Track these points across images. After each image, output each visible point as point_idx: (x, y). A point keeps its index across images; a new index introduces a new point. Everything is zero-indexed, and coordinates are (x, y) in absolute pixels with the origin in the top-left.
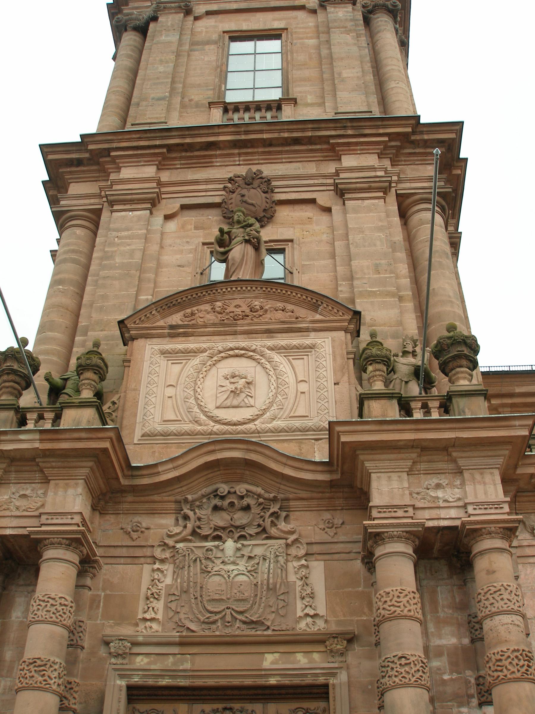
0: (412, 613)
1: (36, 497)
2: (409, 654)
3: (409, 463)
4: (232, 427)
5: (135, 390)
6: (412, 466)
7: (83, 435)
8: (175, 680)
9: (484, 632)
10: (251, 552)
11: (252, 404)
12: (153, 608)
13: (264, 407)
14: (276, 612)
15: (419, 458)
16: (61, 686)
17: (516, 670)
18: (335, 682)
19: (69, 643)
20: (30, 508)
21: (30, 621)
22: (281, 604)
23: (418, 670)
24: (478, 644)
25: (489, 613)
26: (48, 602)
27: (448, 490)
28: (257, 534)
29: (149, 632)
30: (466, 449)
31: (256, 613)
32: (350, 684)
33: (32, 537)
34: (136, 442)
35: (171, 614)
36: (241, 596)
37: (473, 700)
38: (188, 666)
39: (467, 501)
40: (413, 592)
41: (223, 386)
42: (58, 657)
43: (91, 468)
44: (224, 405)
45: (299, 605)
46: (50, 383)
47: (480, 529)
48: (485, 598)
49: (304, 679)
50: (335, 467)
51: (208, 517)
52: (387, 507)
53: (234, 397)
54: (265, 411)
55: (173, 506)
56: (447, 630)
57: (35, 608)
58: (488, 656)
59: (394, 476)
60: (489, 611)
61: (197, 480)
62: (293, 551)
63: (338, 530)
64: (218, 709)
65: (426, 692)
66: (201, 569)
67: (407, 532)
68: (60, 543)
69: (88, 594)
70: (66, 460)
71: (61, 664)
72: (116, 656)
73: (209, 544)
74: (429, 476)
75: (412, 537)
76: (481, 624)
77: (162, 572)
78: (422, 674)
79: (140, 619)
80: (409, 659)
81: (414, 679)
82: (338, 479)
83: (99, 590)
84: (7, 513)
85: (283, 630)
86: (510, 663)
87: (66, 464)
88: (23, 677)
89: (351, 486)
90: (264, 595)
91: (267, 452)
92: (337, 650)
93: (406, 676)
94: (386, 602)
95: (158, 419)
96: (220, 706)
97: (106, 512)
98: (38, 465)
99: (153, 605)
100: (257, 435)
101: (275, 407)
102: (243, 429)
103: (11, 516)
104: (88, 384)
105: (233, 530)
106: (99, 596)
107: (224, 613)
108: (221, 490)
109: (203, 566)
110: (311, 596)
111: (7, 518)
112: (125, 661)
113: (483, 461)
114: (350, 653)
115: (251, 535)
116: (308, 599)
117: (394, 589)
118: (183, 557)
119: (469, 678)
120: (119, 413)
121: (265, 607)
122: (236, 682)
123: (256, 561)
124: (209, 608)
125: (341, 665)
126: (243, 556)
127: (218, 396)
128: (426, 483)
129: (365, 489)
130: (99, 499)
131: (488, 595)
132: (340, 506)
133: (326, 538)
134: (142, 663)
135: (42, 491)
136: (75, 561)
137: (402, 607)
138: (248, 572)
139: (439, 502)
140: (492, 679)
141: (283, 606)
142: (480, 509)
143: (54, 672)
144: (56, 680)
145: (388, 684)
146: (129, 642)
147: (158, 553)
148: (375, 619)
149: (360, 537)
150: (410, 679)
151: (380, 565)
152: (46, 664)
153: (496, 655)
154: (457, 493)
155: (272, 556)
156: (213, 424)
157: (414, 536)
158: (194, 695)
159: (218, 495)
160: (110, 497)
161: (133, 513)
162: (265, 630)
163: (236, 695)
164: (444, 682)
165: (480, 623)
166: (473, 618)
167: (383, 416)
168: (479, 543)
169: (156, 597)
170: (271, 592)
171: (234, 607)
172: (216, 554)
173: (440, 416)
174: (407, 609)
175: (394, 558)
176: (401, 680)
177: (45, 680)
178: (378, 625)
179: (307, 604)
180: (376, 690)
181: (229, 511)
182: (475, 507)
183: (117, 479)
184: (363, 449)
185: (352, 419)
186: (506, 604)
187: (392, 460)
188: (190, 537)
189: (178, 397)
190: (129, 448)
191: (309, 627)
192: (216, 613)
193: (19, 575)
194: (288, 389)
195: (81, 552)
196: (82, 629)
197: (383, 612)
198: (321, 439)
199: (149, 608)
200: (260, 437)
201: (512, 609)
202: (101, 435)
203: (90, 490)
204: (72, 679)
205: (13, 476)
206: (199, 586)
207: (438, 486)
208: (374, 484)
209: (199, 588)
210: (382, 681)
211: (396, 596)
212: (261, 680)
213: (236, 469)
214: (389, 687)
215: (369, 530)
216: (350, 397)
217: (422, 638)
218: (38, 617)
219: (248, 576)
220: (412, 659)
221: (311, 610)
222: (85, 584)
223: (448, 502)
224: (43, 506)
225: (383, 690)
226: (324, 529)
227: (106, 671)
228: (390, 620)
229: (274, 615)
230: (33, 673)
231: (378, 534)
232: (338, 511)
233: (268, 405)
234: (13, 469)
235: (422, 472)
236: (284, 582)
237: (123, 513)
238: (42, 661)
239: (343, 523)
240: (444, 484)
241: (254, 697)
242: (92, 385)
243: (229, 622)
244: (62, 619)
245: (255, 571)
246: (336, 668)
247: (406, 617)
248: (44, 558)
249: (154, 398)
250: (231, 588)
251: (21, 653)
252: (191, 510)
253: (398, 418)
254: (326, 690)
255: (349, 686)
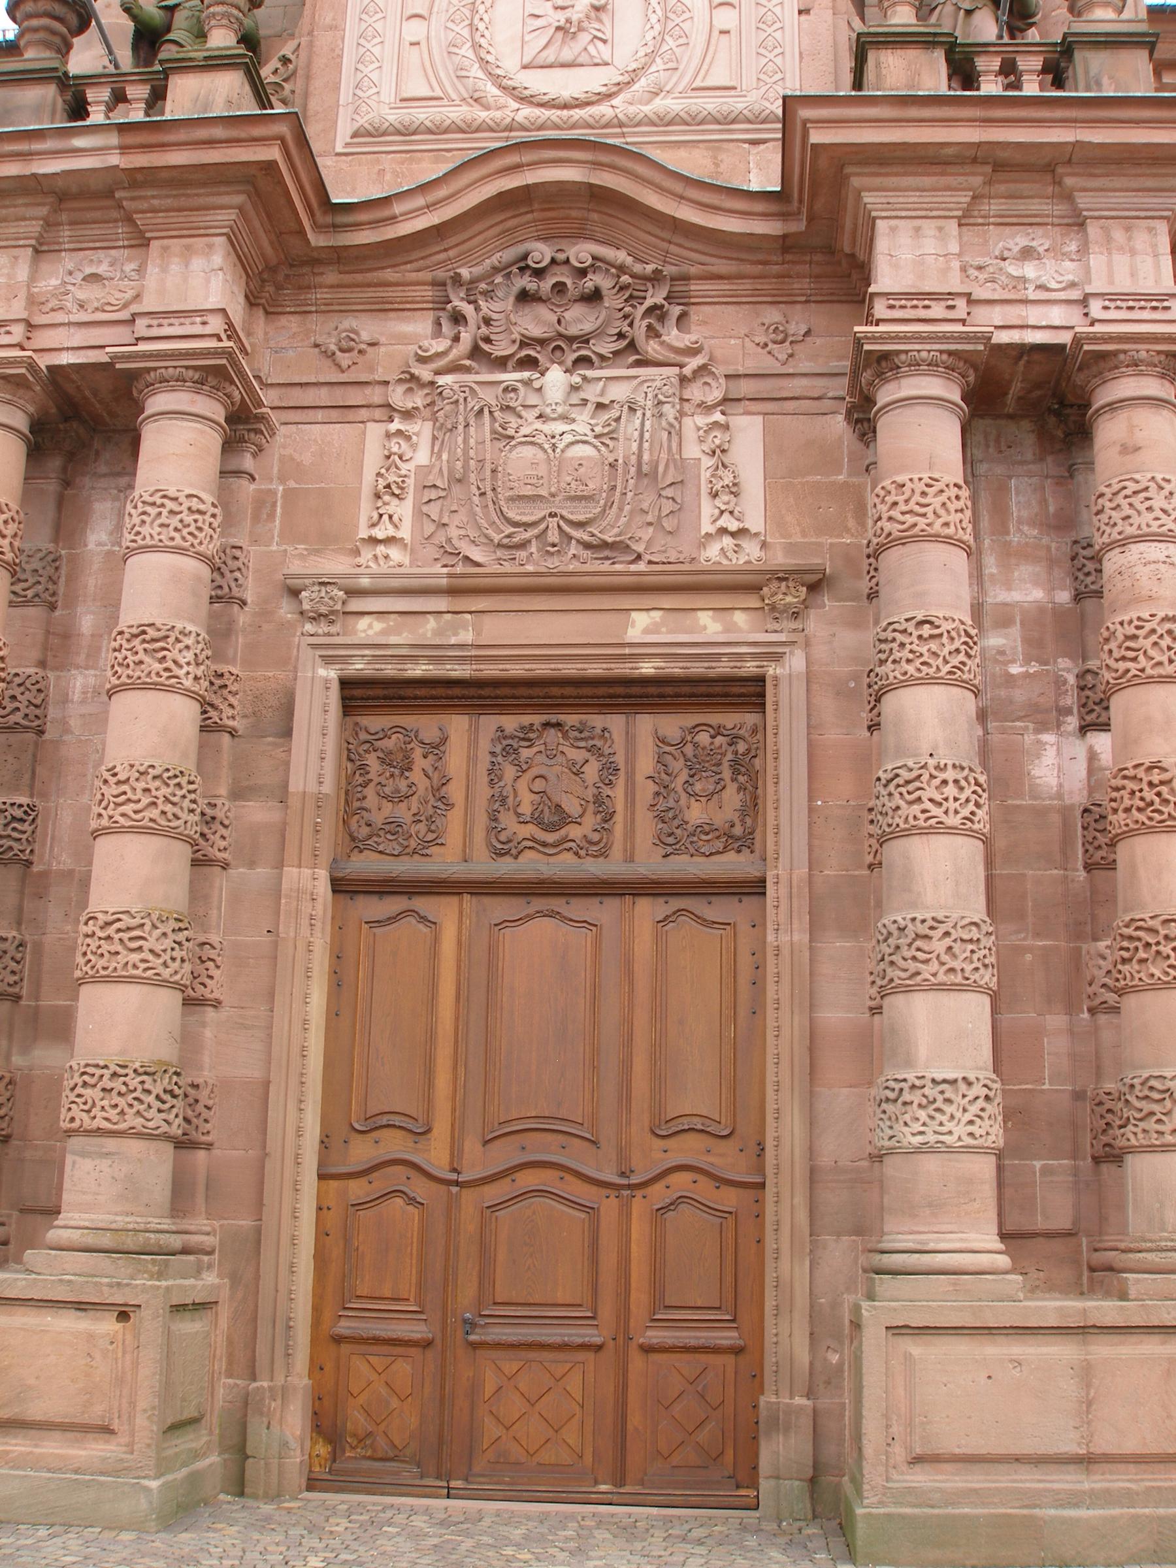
0: (951, 531)
1: (121, 279)
2: (941, 616)
3: (964, 198)
4: (559, 112)
5: (332, 28)
6: (969, 204)
7: (219, 132)
8: (440, 667)
9: (1105, 575)
10: (602, 394)
11: (607, 58)
12: (390, 517)
13: (634, 66)
14: (657, 524)
15: (987, 188)
16: (202, 681)
17: (1165, 659)
18: (778, 671)
19: (213, 593)
20: (109, 304)
21: (128, 548)
22: (668, 506)
23: (958, 651)
24: (1089, 604)
25: (1120, 537)
26: (163, 505)
27: (1049, 263)
28: (616, 353)
29: (384, 568)
30: (1097, 171)
31: (613, 527)
32: (809, 677)
33: (118, 366)
34: (339, 149)
35: (429, 528)
36: (580, 490)
37: (1069, 719)
38: (466, 636)
39: (1088, 290)
40: (956, 485)
41: (538, 16)
42: (192, 621)
43: (241, 208)
44: (540, 60)
45: (707, 509)
46: (134, 18)
47: (1115, 353)
48: (1113, 505)
49: (714, 664)
50: (796, 204)
51: (507, 318)
52: (909, 296)
53: (563, 42)
54: (634, 76)
55: (428, 292)
56: (1025, 571)
57: (136, 520)
58: (1108, 628)
59: (929, 227)
60: (1120, 533)
61: (480, 233)
62: (696, 392)
63: (796, 347)
64: (532, 725)
65: (972, 696)
66: (493, 431)
67: (950, 353)
68: (181, 379)
69: (248, 489)
70: (181, 191)
71: (198, 635)
72: (314, 619)
73: (511, 377)
74: (1008, 229)
75: (961, 364)
76: (1100, 561)
77: (408, 438)
78: (965, 659)
79: (363, 539)
80: (938, 627)
81: (947, 668)
82: (801, 233)
83: (271, 480)
84: (60, 317)
85: (669, 563)
86: (1155, 644)
87: (183, 202)
88: (120, 665)
89: (830, 250)
90: (630, 488)
91: (640, 169)
92: (785, 605)
93: (930, 661)
94: (895, 504)
95: (388, 95)
96: (537, 719)
97: (280, 310)
98: (120, 207)
99: (390, 509)
100: (618, 130)
101: (659, 64)
102: (586, 117)
103: (70, 324)
104: (223, 15)
105: (563, 346)
106: (273, 493)
107: (543, 526)
108: (536, 255)
109: (497, 425)
110: (734, 490)
111: (61, 329)
112: (333, 629)
113: (1135, 200)
114: (812, 613)
115: (602, 358)
116: (725, 498)
117: (916, 477)
118: (453, 406)
119: (1065, 674)
120: (299, 84)
121: (632, 512)
122: (570, 669)
123: (614, 413)
124: (511, 514)
125: (792, 637)
126: (585, 402)
127: (527, 38)
128: (1001, 245)
129: (861, 256)
130: (263, 281)
131: (1120, 499)
132: (802, 295)
133: (769, 364)
134: (371, 632)
135: (133, 266)
136: (215, 417)
137: (931, 515)
138: (596, 437)
139: (1026, 289)
140: (1114, 675)
141: (672, 512)
142: (1117, 308)
143: (185, 653)
144: (191, 669)
145: (891, 677)
146: (340, 590)
147: (398, 397)
148: (869, 542)
149: (846, 365)
150: (938, 667)
151: (884, 425)
152: (168, 637)
153: (1126, 625)
154: (1069, 270)
155: (649, 403)
156: (516, 105)
157: (965, 362)
158: (480, 697)
159: (528, 267)
160: (287, 276)
161: (341, 311)
162: (632, 562)
163: (570, 697)
164: (1010, 679)
165: (1097, 559)
166: (1084, 548)
167: (912, 87)
168: (1109, 384)
169: (397, 492)
170: (646, 481)
171: (564, 513)
172: (525, 398)
173: (1041, 90)
174: (941, 521)
175: (919, 409)
176: (919, 670)
177: (167, 670)
178: (876, 555)
179: (723, 508)
180: (866, 691)
181: (553, 304)
182: (1107, 303)
183: (302, 232)
184: (860, 163)
185: (837, 90)
186: (1157, 519)
187: (925, 190)
188: (467, 362)
189: (434, 42)
190: (325, 164)
191: (727, 557)
192: (527, 526)
193: (97, 453)
194: (689, 21)
195: (229, 396)
196: (239, 564)
197: (888, 527)
198: (764, 141)
199: (381, 516)
200: (623, 135)
201: (1170, 531)
202: (258, 131)
203: (242, 260)
204: (223, 668)
205: (67, 233)
206: (488, 467)
207: (1027, 254)
208: (882, 245)
209: (488, 473)
210: (880, 670)
211: (918, 492)
212: (622, 666)
213: (570, 208)
214: (892, 684)
215: (866, 347)
216: (835, 44)
217: (971, 585)
218: (144, 538)
219: (595, 447)
220: (946, 626)
221: (733, 520)
222: (242, 469)
223: (1048, 290)
224: (137, 297)
225: (880, 689)
226: (766, 345)
227: (295, 651)
228: (903, 544)
229: (651, 529)
230: (141, 656)
231: (885, 356)
232: (798, 307)
233: (643, 60)
234: (64, 217)
235: (992, 220)
236: (675, 460)
237: (316, 312)
238: (159, 630)
239: (808, 333)
240: (1041, 249)
241: (608, 701)
242: (233, 16)
243: (554, 545)
244: (196, 542)
245: (612, 435)
246: (783, 644)
247: (936, 538)
248: (147, 412)
249: (379, 47)
250: (559, 472)
251: (115, 618)
252: (469, 303)
253: (943, 90)
254: (759, 689)
255: (808, 682)
